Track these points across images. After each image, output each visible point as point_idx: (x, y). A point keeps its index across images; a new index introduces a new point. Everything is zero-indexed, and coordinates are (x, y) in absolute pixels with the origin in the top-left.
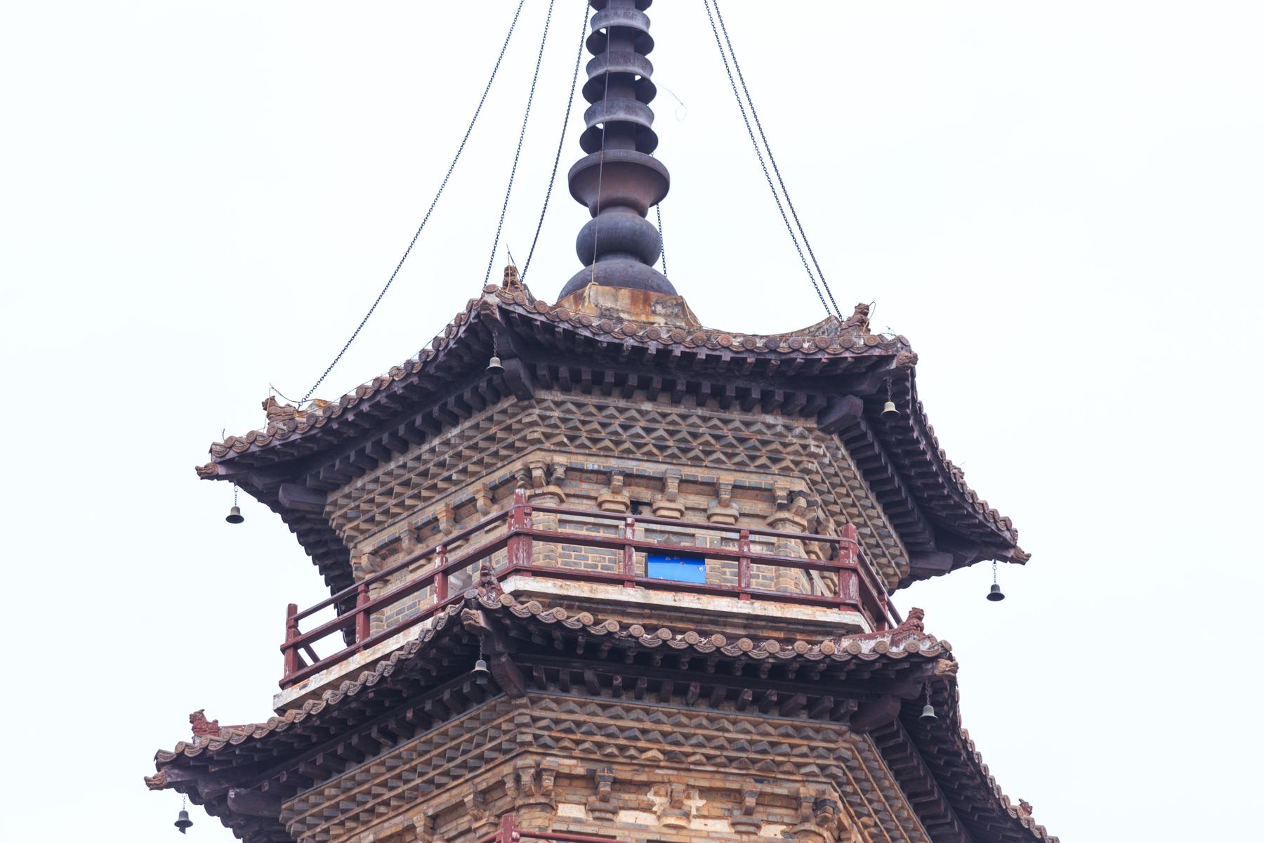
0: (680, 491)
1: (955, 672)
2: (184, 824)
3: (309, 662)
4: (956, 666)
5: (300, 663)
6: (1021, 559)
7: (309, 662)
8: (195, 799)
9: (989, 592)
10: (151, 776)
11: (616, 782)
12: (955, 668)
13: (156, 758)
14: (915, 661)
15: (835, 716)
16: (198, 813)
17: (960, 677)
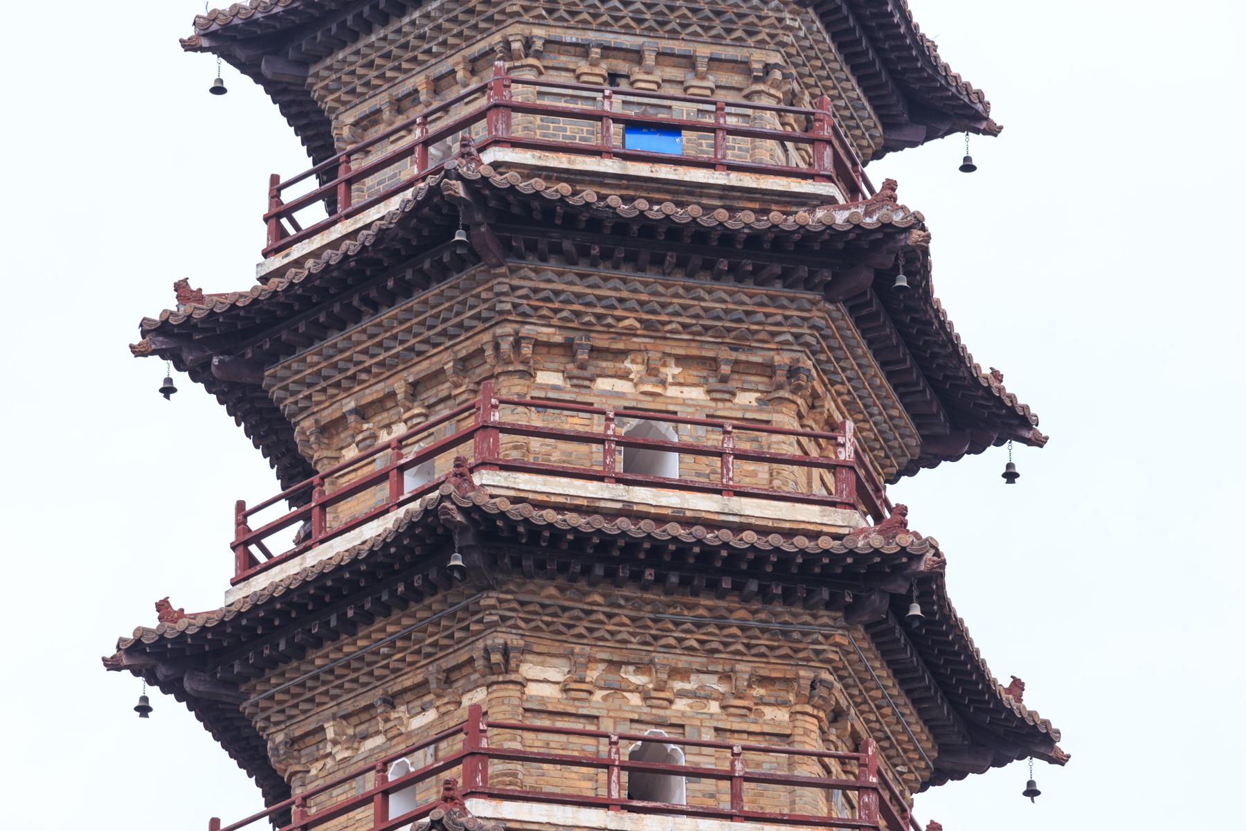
0: (657, 63)
1: (928, 242)
2: (144, 709)
3: (262, 559)
4: (929, 237)
5: (252, 561)
6: (994, 131)
7: (262, 559)
8: (151, 681)
9: (1025, 788)
10: (109, 656)
11: (593, 349)
12: (928, 238)
13: (141, 325)
14: (889, 231)
15: (809, 285)
16: (182, 379)
17: (932, 246)
